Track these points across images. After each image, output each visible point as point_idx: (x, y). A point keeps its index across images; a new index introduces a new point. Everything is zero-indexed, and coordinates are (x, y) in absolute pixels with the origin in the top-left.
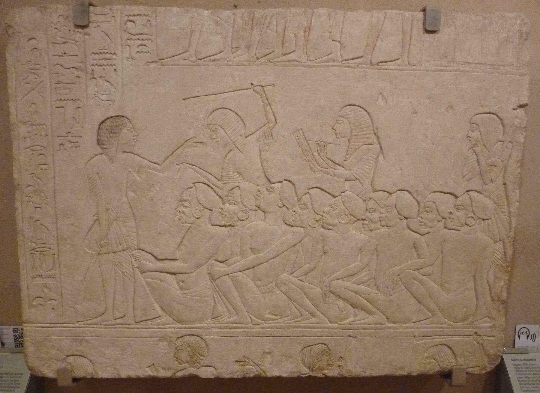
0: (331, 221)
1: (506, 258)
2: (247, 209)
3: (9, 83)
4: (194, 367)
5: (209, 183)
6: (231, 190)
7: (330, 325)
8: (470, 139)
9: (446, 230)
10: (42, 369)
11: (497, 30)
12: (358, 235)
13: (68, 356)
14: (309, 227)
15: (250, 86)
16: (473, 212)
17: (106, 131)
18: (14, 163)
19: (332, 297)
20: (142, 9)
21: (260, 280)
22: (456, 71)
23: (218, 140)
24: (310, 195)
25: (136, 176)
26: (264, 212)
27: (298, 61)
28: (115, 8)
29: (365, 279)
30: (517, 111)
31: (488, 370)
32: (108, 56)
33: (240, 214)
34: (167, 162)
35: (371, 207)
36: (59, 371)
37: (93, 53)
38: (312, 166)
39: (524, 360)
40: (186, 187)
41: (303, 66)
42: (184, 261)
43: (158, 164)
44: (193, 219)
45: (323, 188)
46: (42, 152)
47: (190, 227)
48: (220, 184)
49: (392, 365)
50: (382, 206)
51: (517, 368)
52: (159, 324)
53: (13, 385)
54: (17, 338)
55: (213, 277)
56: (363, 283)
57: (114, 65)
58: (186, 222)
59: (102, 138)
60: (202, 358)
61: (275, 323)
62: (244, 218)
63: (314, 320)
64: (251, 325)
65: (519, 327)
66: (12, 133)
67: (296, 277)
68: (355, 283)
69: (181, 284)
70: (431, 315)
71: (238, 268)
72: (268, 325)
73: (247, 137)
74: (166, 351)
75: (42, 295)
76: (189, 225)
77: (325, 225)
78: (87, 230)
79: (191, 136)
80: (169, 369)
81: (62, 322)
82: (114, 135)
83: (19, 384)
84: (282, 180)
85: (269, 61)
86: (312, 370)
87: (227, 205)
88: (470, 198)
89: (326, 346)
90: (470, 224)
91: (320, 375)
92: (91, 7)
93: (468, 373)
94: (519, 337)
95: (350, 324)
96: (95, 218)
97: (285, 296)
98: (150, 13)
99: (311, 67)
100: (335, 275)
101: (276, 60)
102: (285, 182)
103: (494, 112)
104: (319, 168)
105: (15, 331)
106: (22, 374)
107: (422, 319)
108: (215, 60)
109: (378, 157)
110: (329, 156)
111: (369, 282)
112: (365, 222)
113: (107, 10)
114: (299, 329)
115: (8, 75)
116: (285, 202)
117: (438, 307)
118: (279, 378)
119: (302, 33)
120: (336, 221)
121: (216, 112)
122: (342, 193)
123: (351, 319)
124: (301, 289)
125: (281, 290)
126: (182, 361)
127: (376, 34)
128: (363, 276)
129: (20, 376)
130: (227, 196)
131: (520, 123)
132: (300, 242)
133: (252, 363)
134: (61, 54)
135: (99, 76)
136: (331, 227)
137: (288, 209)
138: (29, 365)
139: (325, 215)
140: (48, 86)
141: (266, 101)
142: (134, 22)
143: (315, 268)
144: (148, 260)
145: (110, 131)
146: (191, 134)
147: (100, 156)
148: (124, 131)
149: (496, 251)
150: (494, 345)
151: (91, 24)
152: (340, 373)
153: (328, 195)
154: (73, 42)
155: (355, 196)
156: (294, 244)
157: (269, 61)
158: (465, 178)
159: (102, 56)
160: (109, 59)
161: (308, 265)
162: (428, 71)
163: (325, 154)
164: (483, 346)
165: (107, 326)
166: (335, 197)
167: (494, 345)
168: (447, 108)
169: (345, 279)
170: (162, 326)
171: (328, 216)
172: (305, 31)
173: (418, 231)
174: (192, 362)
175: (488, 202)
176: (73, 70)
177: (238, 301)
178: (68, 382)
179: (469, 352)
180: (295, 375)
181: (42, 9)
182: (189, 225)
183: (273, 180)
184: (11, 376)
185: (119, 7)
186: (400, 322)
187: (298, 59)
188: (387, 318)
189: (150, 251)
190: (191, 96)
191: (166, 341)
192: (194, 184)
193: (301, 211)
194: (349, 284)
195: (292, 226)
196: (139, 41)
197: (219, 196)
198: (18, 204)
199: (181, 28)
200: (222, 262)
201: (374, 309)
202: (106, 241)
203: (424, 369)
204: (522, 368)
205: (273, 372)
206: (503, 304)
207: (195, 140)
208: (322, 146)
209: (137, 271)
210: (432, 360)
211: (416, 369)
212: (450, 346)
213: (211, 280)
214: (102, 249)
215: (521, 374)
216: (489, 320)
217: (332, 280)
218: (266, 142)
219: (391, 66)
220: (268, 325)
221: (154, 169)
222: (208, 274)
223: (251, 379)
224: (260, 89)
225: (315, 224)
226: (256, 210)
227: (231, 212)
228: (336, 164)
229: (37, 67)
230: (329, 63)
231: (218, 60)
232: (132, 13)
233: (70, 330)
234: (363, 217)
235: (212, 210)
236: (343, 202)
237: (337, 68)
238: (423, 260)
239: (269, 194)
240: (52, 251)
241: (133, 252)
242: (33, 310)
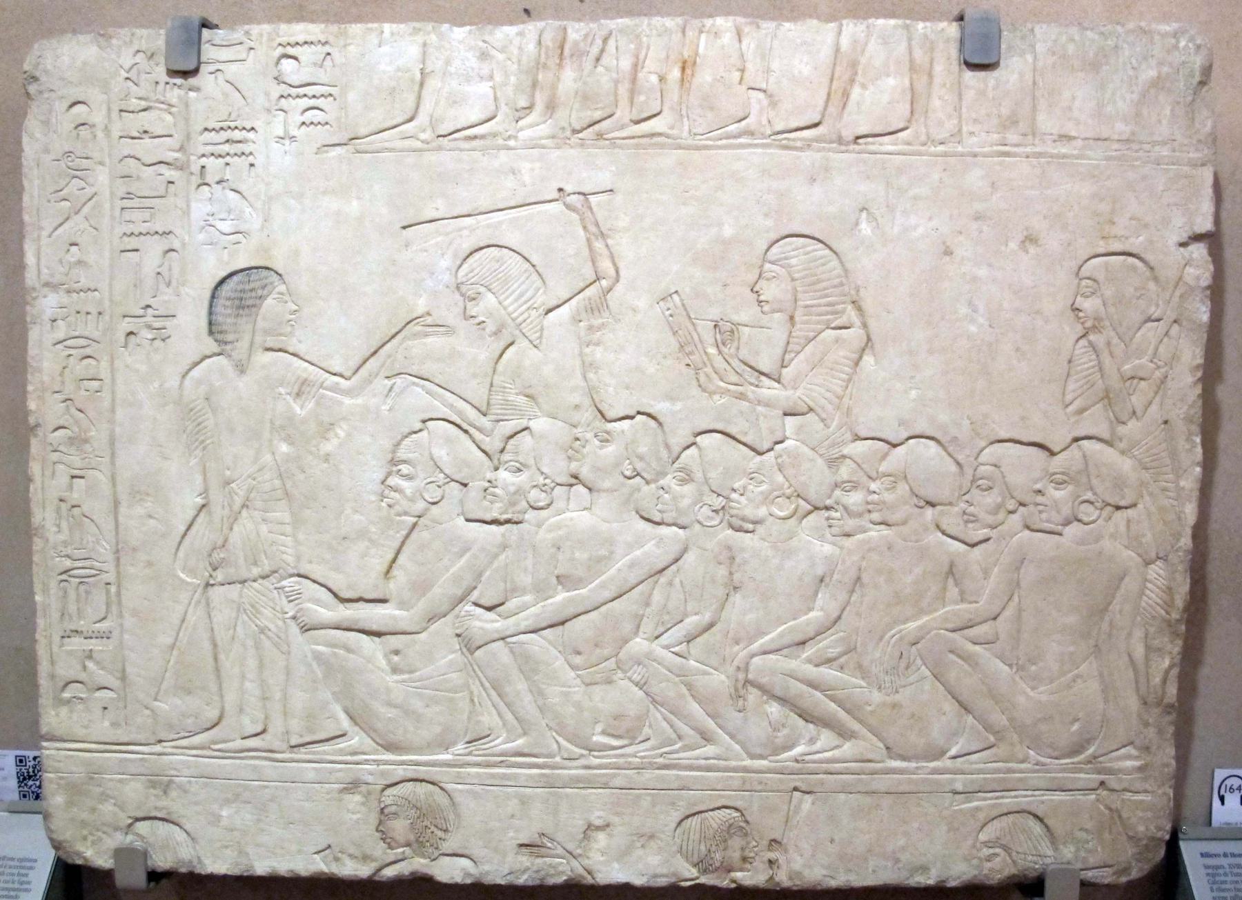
0: (749, 512)
1: (1172, 600)
2: (548, 481)
3: (26, 198)
4: (424, 857)
5: (459, 421)
6: (511, 437)
7: (747, 762)
8: (1081, 314)
9: (1027, 532)
10: (80, 847)
11: (1134, 61)
12: (815, 545)
13: (138, 820)
14: (697, 527)
15: (555, 195)
16: (1092, 489)
17: (228, 303)
18: (29, 377)
19: (753, 695)
20: (314, 30)
21: (579, 653)
22: (1039, 155)
23: (482, 319)
24: (700, 448)
25: (294, 405)
26: (590, 489)
27: (668, 136)
28: (255, 29)
29: (833, 652)
30: (1190, 248)
31: (1135, 874)
32: (237, 135)
33: (534, 495)
34: (363, 372)
35: (845, 477)
36: (119, 853)
37: (206, 129)
38: (702, 378)
39: (1233, 855)
40: (407, 430)
41: (680, 147)
42: (402, 605)
43: (341, 376)
44: (421, 505)
45: (733, 430)
46: (88, 351)
47: (415, 525)
48: (485, 422)
49: (897, 861)
50: (874, 475)
51: (1214, 875)
52: (342, 752)
53: (16, 886)
54: (24, 779)
55: (469, 645)
56: (829, 661)
57: (251, 153)
58: (406, 513)
59: (220, 319)
60: (440, 834)
61: (616, 756)
62: (541, 504)
63: (710, 750)
64: (558, 759)
65: (1220, 774)
66: (28, 308)
67: (667, 647)
68: (809, 661)
69: (396, 658)
70: (992, 738)
71: (526, 623)
72: (598, 761)
73: (550, 311)
74: (359, 816)
75: (82, 676)
76: (415, 520)
77: (735, 521)
78: (183, 528)
79: (420, 310)
80: (366, 858)
81: (126, 740)
82: (246, 311)
83: (29, 883)
84: (632, 413)
85: (600, 136)
86: (705, 872)
87: (503, 475)
88: (1084, 456)
89: (738, 814)
90: (1086, 519)
91: (725, 883)
92: (205, 31)
93: (1084, 884)
94: (1222, 799)
95: (797, 761)
96: (200, 501)
97: (641, 693)
98: (331, 39)
99: (698, 148)
100: (761, 641)
101: (617, 134)
102: (639, 417)
104: (722, 384)
105: (21, 761)
106: (36, 861)
107: (974, 749)
108: (475, 137)
109: (861, 357)
110: (744, 353)
111: (842, 660)
113: (238, 35)
114: (674, 772)
115: (26, 183)
116: (640, 466)
117: (1011, 720)
118: (626, 888)
119: (676, 73)
120: (762, 512)
121: (477, 256)
123: (799, 750)
124: (678, 676)
125: (630, 679)
126: (395, 841)
127: (845, 75)
128: (828, 644)
129: (28, 864)
130: (502, 451)
131: (1198, 278)
132: (677, 560)
133: (560, 851)
134: (137, 135)
135: (217, 179)
136: (750, 527)
137: (648, 483)
138: (54, 836)
139: (734, 496)
140: (107, 206)
141: (593, 229)
142: (296, 58)
143: (711, 625)
144: (318, 602)
145: (237, 302)
146: (421, 305)
147: (215, 359)
148: (269, 301)
149: (1149, 585)
150: (1149, 814)
151: (204, 69)
152: (771, 878)
153: (741, 446)
154: (162, 106)
155: (806, 449)
156: (660, 566)
157: (600, 136)
158: (1071, 408)
159: (224, 135)
160: (240, 142)
161: (695, 618)
162: (975, 156)
163: (732, 350)
164: (1120, 817)
165: (225, 754)
166: (760, 454)
167: (1149, 814)
168: (1023, 242)
169: (785, 651)
170: (349, 758)
171: (743, 499)
172: (683, 69)
173: (962, 536)
174: (419, 844)
176: (162, 169)
177: (527, 704)
178: (138, 880)
179: (1086, 831)
180: (662, 882)
181: (100, 39)
182: (415, 520)
183: (611, 414)
184: (12, 863)
185: (266, 28)
186: (917, 758)
187: (670, 132)
188: (888, 748)
189: (321, 580)
190: (422, 220)
191: (360, 793)
192: (424, 422)
193: (678, 488)
194: (793, 664)
195: (658, 524)
196: (306, 99)
197: (484, 451)
198: (35, 468)
199: (399, 69)
200: (489, 609)
201: (856, 726)
202: (222, 555)
203: (976, 872)
204: (1226, 874)
205: (612, 873)
206: (1169, 713)
207: (429, 320)
208: (726, 332)
209: (294, 629)
210: (997, 850)
211: (958, 872)
212: (1039, 814)
213: (465, 650)
214: (214, 574)
215: (1223, 890)
216: (1134, 752)
217: (753, 656)
218: (597, 322)
219: (887, 144)
220: (598, 761)
221: (334, 388)
222: (458, 635)
223: (554, 888)
224: (579, 202)
225: (712, 518)
226: (571, 485)
227: (512, 489)
229: (85, 163)
230: (742, 140)
231: (483, 137)
232: (292, 40)
233: (141, 759)
234: (828, 502)
235: (465, 485)
236: (778, 464)
237: (760, 150)
238: (974, 605)
239: (601, 448)
240: (104, 576)
241: (284, 583)
242: (64, 711)
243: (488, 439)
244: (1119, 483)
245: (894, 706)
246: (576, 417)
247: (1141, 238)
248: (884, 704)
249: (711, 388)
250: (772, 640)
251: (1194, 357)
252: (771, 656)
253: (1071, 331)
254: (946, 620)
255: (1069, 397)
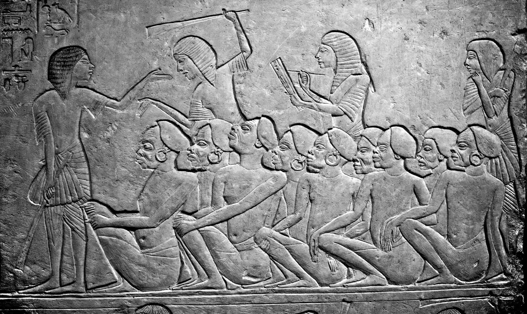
19: (321, 254)
29: (359, 231)
38: (293, 99)
45: (307, 123)
52: (115, 291)
68: (348, 236)
71: (209, 220)
84: (259, 115)
88: (474, 134)
90: (476, 164)
103: (491, 37)
111: (363, 235)
112: (357, 163)
122: (329, 129)
124: (284, 245)
136: (318, 170)
141: (240, 28)
144: (103, 213)
146: (155, 65)
168: (441, 34)
169: (336, 231)
175: (494, 137)
192: (157, 121)
194: (340, 237)
208: (305, 77)
221: (113, 106)
226: (230, 152)
228: (321, 96)
241: (86, 204)
243: (189, 129)
244: (491, 145)
245: (390, 257)
246: (233, 119)
247: (494, 32)
248: (384, 256)
249: (297, 103)
250: (329, 225)
251: (521, 87)
252: (329, 234)
253: (465, 74)
254: (413, 214)
255: (466, 106)
